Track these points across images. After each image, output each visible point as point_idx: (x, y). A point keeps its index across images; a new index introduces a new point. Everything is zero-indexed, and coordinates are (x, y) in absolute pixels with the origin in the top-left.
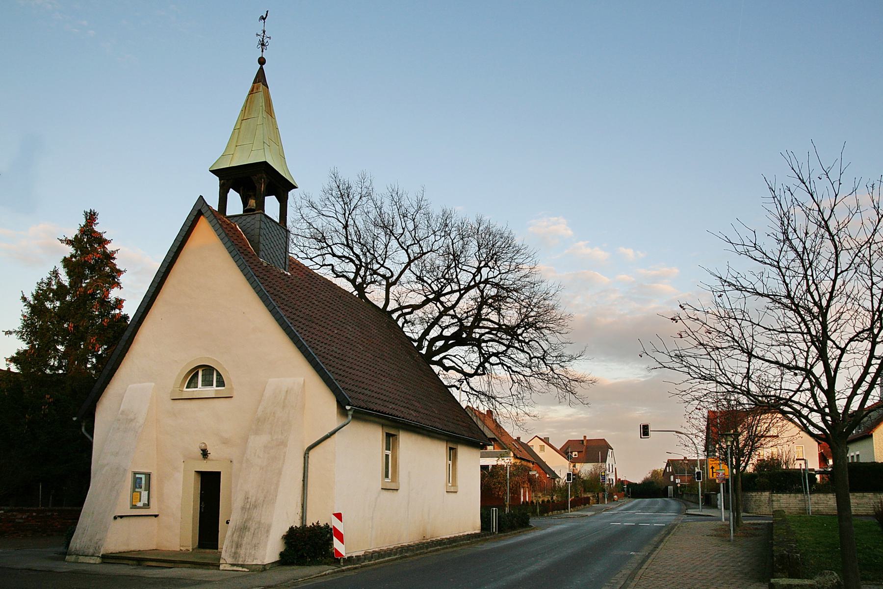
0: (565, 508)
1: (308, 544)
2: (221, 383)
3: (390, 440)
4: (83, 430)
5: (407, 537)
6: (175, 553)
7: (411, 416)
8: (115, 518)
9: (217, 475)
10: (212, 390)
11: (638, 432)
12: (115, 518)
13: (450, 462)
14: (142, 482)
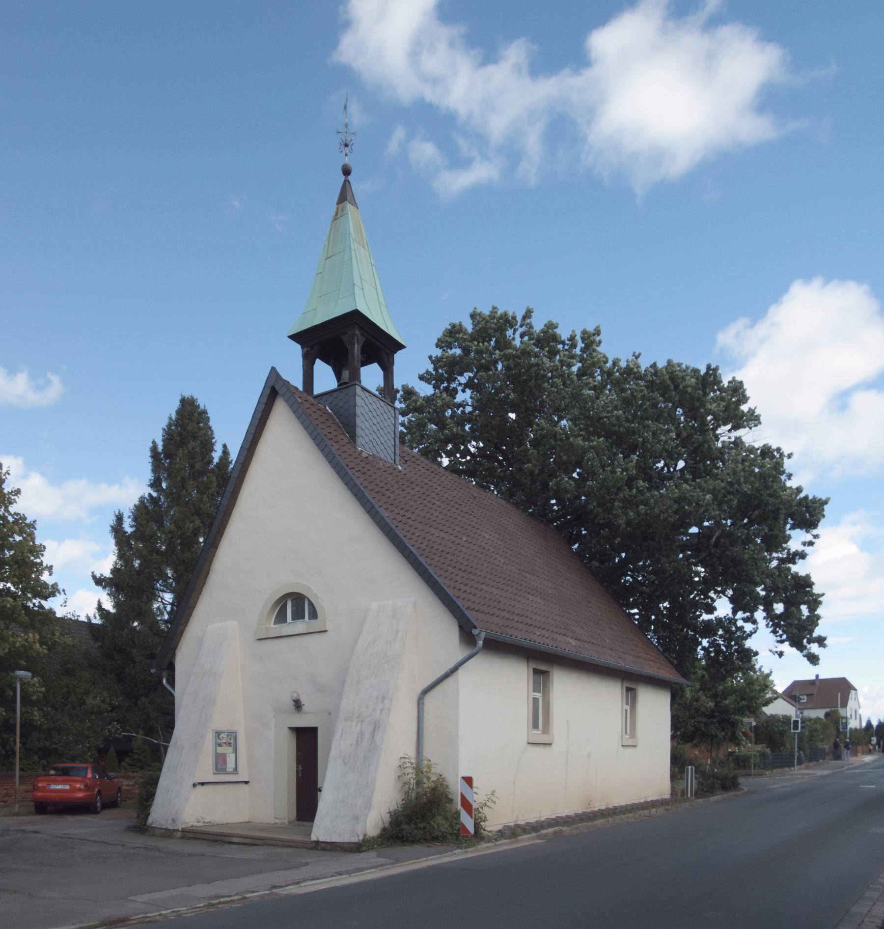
0: (792, 765)
1: (426, 814)
2: (314, 615)
3: (541, 677)
4: (164, 681)
5: (568, 806)
7: (569, 646)
8: (194, 785)
10: (300, 626)
11: (304, 701)
12: (194, 785)
13: (538, 695)
14: (228, 739)
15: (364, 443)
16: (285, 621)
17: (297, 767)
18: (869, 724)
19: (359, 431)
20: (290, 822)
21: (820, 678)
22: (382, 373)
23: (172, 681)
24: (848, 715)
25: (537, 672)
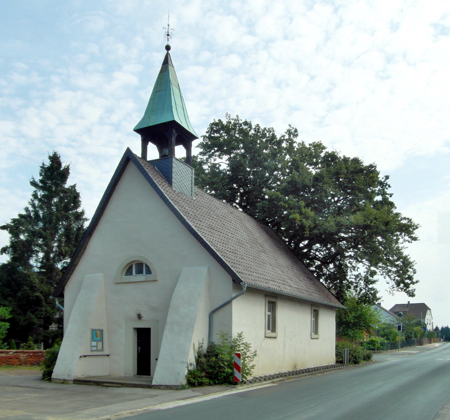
2: (149, 271)
3: (272, 307)
6: (120, 378)
9: (148, 331)
10: (141, 277)
11: (143, 315)
15: (176, 186)
16: (131, 274)
17: (138, 347)
18: (437, 328)
19: (174, 180)
20: (134, 376)
21: (410, 303)
22: (185, 151)
23: (62, 303)
24: (426, 323)
25: (270, 303)
